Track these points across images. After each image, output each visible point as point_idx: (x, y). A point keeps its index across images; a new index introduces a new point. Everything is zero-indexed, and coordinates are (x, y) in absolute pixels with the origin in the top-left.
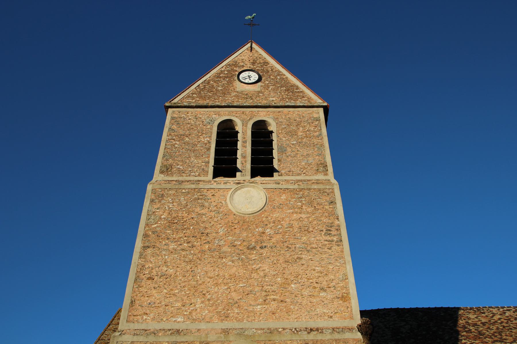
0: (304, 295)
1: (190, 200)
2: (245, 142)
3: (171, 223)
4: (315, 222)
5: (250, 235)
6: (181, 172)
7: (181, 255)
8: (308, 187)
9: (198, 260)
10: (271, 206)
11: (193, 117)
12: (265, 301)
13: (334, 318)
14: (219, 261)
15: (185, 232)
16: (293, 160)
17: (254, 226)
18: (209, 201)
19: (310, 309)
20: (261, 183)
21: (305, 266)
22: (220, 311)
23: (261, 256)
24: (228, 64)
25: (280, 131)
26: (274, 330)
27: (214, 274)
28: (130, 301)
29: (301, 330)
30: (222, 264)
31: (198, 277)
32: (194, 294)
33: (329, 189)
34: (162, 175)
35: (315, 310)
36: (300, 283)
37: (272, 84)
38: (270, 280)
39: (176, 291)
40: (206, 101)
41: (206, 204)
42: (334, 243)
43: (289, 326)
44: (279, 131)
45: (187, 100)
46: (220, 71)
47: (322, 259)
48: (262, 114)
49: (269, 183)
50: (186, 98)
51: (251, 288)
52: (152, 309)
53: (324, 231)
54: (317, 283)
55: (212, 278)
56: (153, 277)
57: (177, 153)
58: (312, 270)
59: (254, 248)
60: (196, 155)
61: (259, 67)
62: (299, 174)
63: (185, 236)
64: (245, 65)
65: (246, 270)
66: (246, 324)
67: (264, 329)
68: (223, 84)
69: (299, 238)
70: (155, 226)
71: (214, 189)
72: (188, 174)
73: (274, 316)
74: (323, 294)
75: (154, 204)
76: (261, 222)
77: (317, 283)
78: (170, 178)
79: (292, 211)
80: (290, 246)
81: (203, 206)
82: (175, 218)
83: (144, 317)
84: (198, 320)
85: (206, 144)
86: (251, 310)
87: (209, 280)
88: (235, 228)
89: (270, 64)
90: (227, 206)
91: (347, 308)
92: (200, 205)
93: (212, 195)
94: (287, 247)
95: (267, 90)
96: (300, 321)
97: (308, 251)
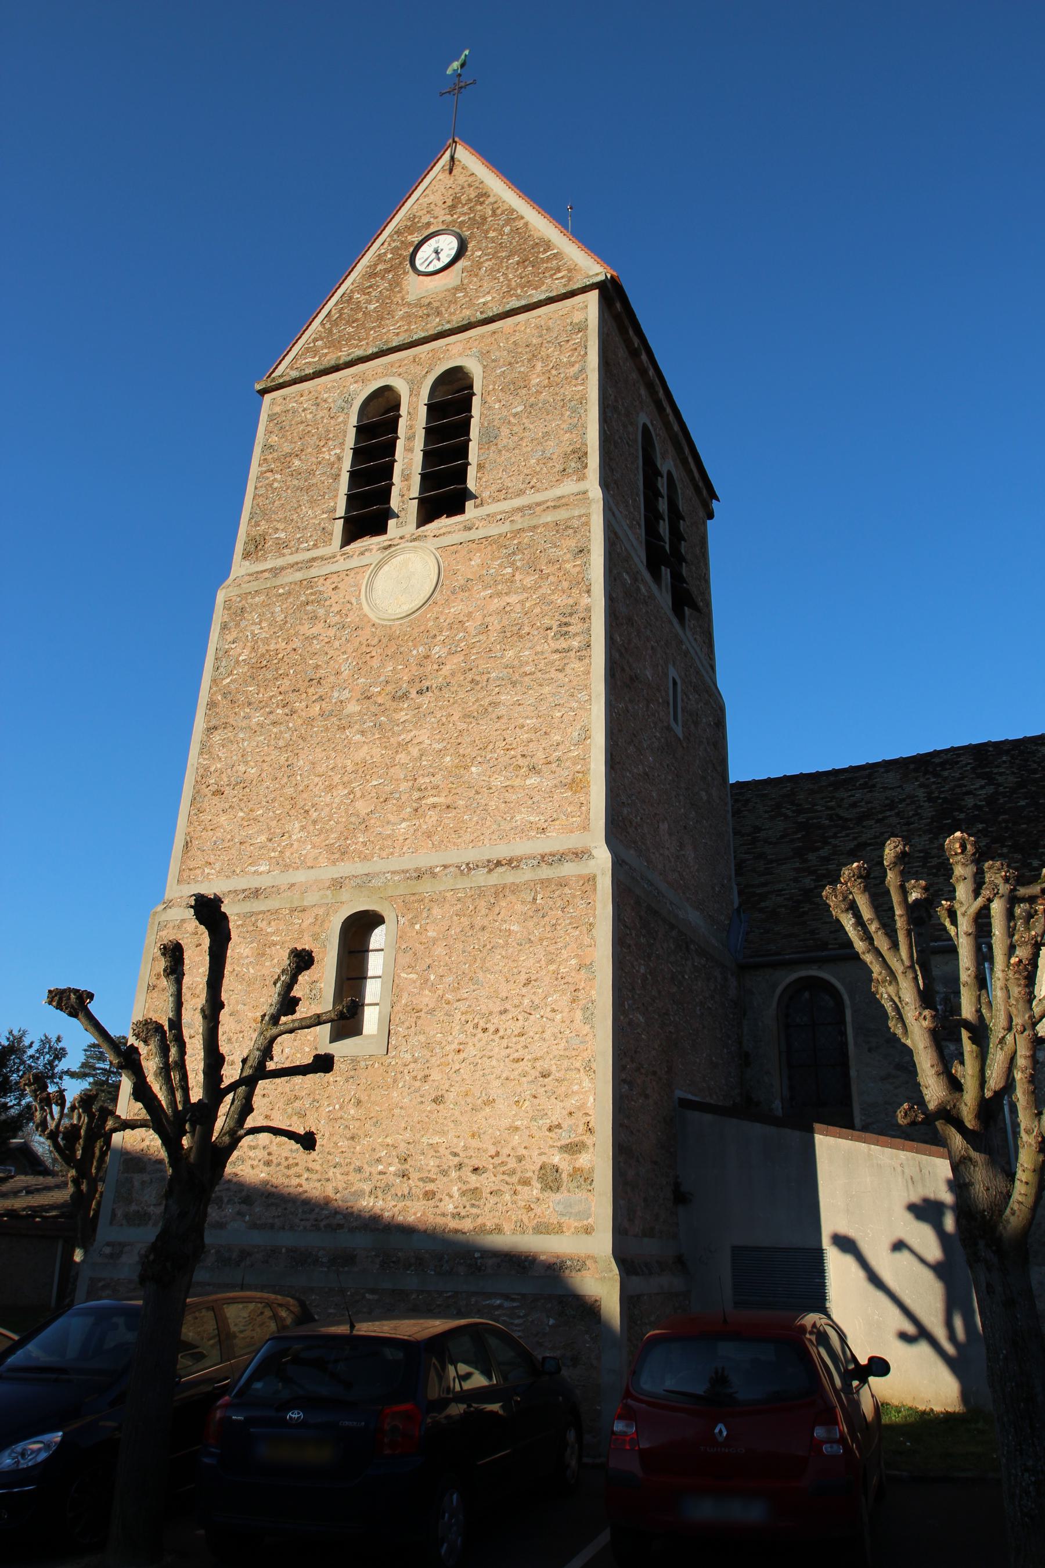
0: (494, 788)
1: (292, 608)
2: (410, 438)
3: (258, 667)
4: (537, 610)
5: (400, 667)
6: (282, 546)
7: (271, 735)
8: (531, 522)
9: (300, 741)
10: (447, 589)
11: (311, 402)
12: (416, 810)
13: (550, 832)
14: (338, 736)
15: (279, 683)
16: (510, 458)
17: (410, 644)
18: (328, 603)
19: (502, 817)
20: (434, 536)
21: (504, 720)
22: (332, 842)
23: (417, 711)
24: (396, 230)
25: (491, 387)
26: (426, 870)
27: (327, 766)
28: (183, 843)
29: (477, 866)
30: (343, 743)
31: (299, 778)
32: (290, 812)
33: (580, 516)
34: (247, 563)
35: (512, 818)
36: (489, 760)
37: (488, 254)
38: (430, 763)
39: (258, 813)
40: (341, 351)
41: (321, 612)
42: (572, 654)
43: (455, 861)
44: (487, 386)
45: (303, 362)
46: (377, 256)
47: (541, 697)
48: (455, 350)
49: (449, 533)
50: (302, 355)
51: (392, 787)
52: (219, 853)
53: (555, 628)
54: (523, 756)
55: (323, 775)
56: (222, 789)
57: (277, 502)
58: (517, 729)
59: (405, 696)
60: (313, 497)
61: (465, 214)
62: (521, 493)
63: (280, 693)
64: (432, 220)
65: (386, 747)
66: (377, 865)
67: (407, 871)
68: (380, 292)
69: (499, 655)
70: (228, 680)
71: (338, 574)
72: (293, 549)
73: (430, 840)
74: (532, 781)
75: (227, 632)
76: (425, 633)
77: (524, 755)
78: (261, 567)
79: (489, 592)
80: (478, 678)
81: (315, 618)
82: (263, 655)
83: (206, 869)
84: (293, 865)
85: (333, 464)
86: (389, 833)
87: (316, 779)
88: (372, 657)
89: (491, 195)
90: (361, 609)
91: (580, 807)
92: (310, 616)
93: (333, 589)
94: (472, 681)
95: (476, 275)
96: (479, 847)
97: (514, 684)
